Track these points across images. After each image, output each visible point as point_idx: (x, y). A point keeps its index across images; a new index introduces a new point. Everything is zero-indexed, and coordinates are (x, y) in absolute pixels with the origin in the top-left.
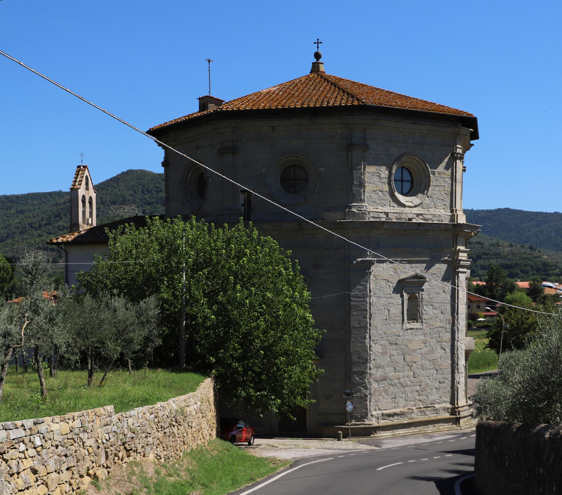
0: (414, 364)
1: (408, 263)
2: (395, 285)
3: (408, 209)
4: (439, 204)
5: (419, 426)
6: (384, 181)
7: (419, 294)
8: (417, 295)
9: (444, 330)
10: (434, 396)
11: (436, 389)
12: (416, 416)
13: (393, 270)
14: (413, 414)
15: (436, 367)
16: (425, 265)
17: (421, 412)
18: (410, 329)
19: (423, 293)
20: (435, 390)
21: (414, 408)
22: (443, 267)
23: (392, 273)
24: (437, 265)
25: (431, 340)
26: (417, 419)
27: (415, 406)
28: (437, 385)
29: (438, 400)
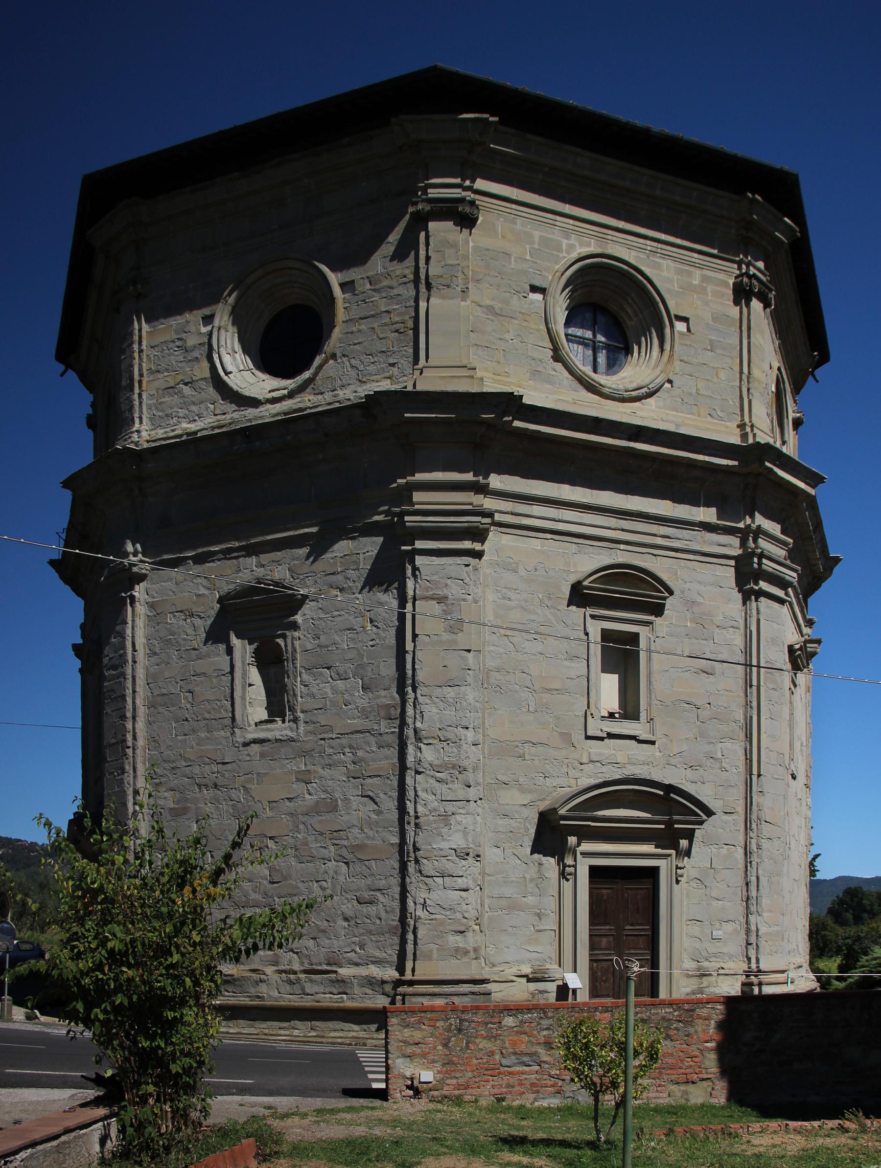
0: (271, 843)
1: (249, 555)
2: (209, 622)
3: (269, 406)
4: (372, 368)
5: (265, 1020)
6: (196, 354)
7: (284, 637)
8: (280, 641)
9: (372, 740)
10: (340, 940)
11: (346, 919)
12: (276, 994)
13: (205, 582)
14: (263, 988)
15: (344, 852)
16: (305, 550)
17: (290, 983)
18: (255, 741)
19: (296, 634)
20: (342, 923)
21: (269, 970)
22: (369, 548)
23: (203, 591)
24: (343, 547)
25: (327, 773)
26: (276, 1000)
27: (275, 963)
28: (349, 908)
29: (352, 955)
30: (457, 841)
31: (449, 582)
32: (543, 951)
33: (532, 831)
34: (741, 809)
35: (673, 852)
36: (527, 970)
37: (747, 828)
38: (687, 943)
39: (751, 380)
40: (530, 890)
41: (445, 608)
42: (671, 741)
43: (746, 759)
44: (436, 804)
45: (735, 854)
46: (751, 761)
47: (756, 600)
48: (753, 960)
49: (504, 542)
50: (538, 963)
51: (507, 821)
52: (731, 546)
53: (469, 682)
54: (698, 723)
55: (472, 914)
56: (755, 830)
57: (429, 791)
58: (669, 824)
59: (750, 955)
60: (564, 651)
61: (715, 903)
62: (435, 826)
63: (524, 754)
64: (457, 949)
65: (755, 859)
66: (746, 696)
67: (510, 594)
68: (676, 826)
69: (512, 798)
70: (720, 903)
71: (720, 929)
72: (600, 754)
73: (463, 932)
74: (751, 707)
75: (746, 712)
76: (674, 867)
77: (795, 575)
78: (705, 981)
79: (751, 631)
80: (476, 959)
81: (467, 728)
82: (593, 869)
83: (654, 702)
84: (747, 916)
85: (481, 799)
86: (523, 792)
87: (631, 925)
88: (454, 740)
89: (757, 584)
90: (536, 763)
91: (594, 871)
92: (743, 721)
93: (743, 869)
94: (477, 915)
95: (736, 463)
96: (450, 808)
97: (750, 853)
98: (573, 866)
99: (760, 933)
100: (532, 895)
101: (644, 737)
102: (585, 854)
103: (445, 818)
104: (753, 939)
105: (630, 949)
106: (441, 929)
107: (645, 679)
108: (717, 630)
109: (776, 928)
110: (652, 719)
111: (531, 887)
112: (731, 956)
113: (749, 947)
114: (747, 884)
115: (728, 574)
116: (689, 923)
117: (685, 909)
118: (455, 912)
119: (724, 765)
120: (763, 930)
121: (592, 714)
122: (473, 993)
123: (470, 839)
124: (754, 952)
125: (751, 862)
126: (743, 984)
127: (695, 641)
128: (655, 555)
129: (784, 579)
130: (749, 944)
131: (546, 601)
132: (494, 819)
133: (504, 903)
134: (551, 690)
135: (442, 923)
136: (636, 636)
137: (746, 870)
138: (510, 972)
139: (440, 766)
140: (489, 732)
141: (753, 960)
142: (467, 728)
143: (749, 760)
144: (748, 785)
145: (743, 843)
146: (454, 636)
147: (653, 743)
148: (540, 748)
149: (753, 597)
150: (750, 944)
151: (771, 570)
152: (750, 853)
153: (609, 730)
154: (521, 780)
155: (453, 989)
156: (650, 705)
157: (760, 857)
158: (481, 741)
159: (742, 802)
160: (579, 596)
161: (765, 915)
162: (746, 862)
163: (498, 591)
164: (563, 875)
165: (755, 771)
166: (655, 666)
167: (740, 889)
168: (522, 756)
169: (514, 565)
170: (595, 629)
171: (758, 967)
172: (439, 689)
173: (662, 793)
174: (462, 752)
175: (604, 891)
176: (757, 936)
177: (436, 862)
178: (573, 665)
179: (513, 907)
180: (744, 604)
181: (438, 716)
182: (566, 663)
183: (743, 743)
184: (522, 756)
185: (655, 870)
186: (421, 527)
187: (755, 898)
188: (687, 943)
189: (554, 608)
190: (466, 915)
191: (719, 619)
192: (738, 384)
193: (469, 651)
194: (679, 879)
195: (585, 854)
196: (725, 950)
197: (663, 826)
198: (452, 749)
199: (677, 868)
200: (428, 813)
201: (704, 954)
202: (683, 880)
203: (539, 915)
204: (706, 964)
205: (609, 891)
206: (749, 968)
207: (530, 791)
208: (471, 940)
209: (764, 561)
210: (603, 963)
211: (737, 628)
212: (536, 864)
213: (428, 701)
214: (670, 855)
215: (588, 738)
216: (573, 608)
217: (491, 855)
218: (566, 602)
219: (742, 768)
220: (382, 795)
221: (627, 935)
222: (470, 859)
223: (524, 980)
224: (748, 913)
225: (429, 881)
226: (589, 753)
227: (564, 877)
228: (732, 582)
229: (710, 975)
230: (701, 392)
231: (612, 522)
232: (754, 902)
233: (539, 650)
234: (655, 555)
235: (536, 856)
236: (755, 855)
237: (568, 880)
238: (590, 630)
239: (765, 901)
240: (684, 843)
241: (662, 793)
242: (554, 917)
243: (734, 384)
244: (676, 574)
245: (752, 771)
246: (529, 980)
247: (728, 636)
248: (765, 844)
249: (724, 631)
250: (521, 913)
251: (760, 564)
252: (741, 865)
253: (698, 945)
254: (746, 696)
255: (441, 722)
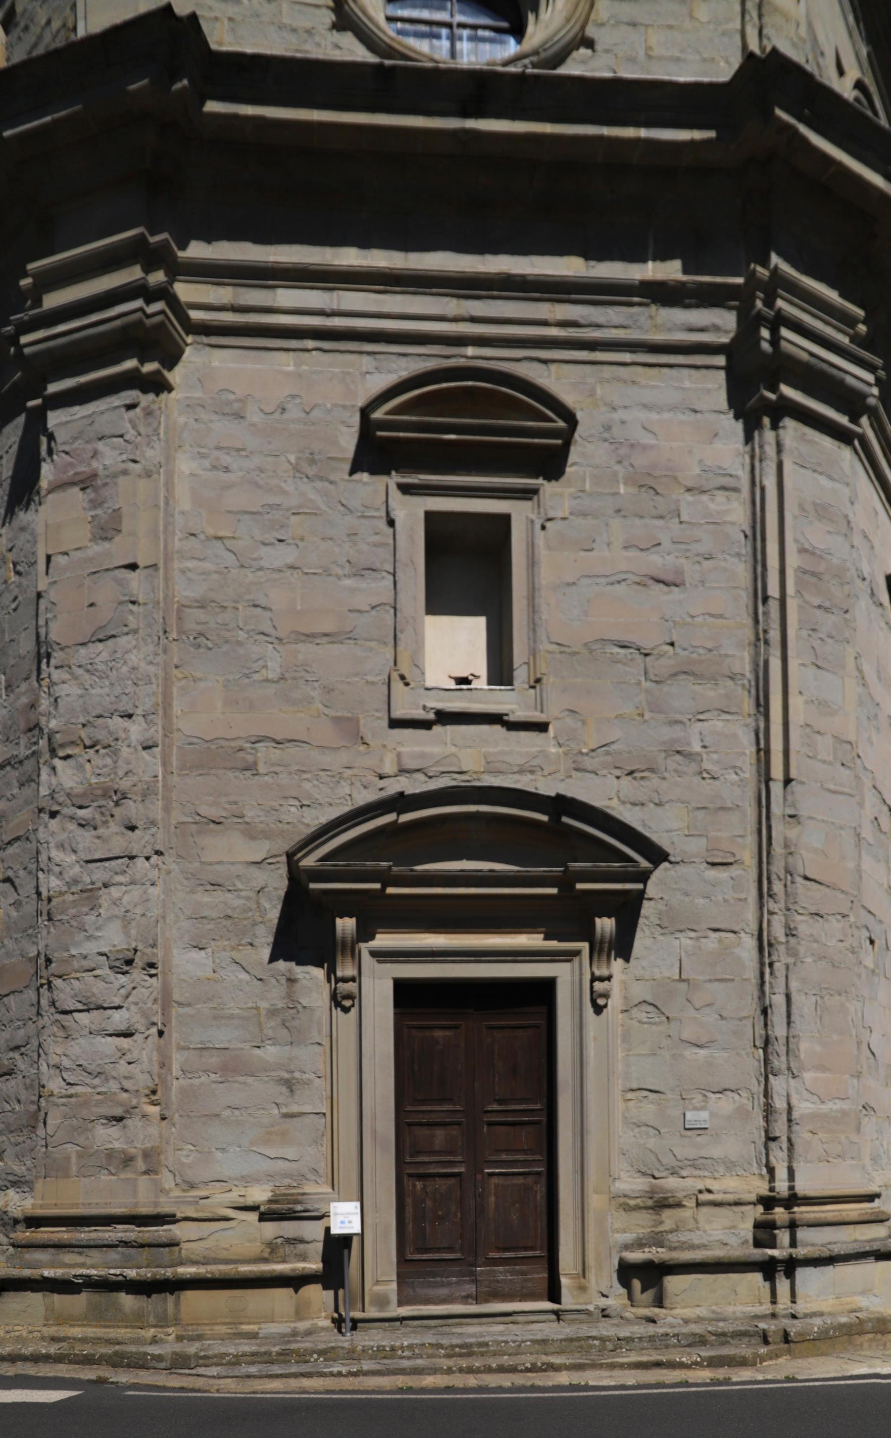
30: (113, 938)
31: (100, 446)
32: (299, 1156)
33: (274, 914)
34: (748, 856)
35: (585, 946)
36: (260, 1194)
37: (763, 893)
38: (624, 1137)
39: (765, 10)
40: (270, 1033)
41: (93, 496)
42: (584, 722)
43: (759, 750)
44: (77, 869)
45: (737, 951)
46: (767, 752)
47: (775, 427)
48: (781, 1173)
49: (215, 364)
50: (287, 1182)
51: (219, 896)
52: (716, 328)
53: (133, 626)
54: (646, 684)
55: (143, 1081)
56: (781, 895)
57: (66, 845)
58: (566, 882)
59: (773, 1161)
60: (343, 560)
61: (690, 1053)
62: (73, 911)
63: (255, 763)
64: (110, 1155)
65: (781, 958)
66: (756, 621)
67: (226, 459)
68: (580, 886)
69: (232, 851)
70: (702, 1052)
71: (703, 1108)
72: (422, 756)
73: (120, 1119)
74: (767, 642)
75: (757, 654)
76: (587, 977)
77: (870, 377)
78: (669, 1218)
79: (763, 489)
80: (146, 1173)
81: (130, 716)
82: (402, 987)
83: (544, 646)
84: (767, 1078)
85: (159, 853)
86: (253, 838)
87: (500, 1102)
88: (106, 742)
89: (774, 389)
90: (284, 779)
91: (405, 992)
92: (749, 675)
93: (754, 980)
94: (151, 1085)
95: (711, 134)
96: (99, 873)
97: (770, 945)
98: (353, 979)
99: (795, 1115)
100: (274, 1041)
101: (520, 715)
102: (381, 955)
103: (89, 895)
104: (780, 1128)
105: (499, 1151)
106: (84, 1113)
107: (524, 602)
108: (689, 497)
109: (838, 1105)
110: (538, 681)
111: (271, 1026)
112: (730, 1166)
113: (772, 1145)
114: (765, 1012)
115: (711, 387)
116: (630, 1095)
117: (620, 1067)
118: (107, 1080)
119: (707, 765)
120: (803, 1107)
121: (402, 677)
122: (126, 1244)
123: (133, 932)
124: (784, 1155)
125: (771, 965)
126: (758, 1225)
127: (637, 521)
128: (545, 362)
129: (842, 382)
130: (770, 1139)
131: (304, 466)
132: (192, 892)
133: (214, 1060)
134: (313, 636)
135: (85, 1104)
136: (505, 520)
137: (762, 983)
138: (220, 1200)
139: (84, 795)
140: (178, 723)
141: (781, 1173)
142: (130, 716)
143: (763, 753)
144: (763, 804)
145: (754, 927)
146: (107, 545)
147: (541, 727)
148: (292, 750)
149: (766, 421)
150: (774, 1139)
151: (805, 356)
152: (770, 945)
153: (440, 706)
154: (250, 814)
155: (93, 1235)
156: (534, 653)
157: (792, 952)
158: (159, 738)
159: (751, 840)
160: (375, 452)
161: (808, 1076)
162: (762, 964)
163: (203, 456)
164: (337, 1001)
165: (777, 772)
166: (546, 576)
167: (748, 1023)
168: (250, 768)
169: (236, 406)
170: (411, 513)
171: (791, 1188)
172: (83, 651)
173: (545, 818)
174: (120, 763)
175: (438, 1034)
176: (790, 1120)
177: (76, 983)
178: (363, 585)
179: (233, 1067)
180: (748, 438)
181: (81, 701)
182: (348, 582)
183: (751, 721)
184: (250, 768)
185: (548, 986)
186: (49, 351)
187: (782, 1041)
188: (624, 1137)
189: (321, 478)
190: (127, 1084)
191: (692, 472)
192: (738, 25)
193: (133, 567)
194: (601, 1002)
195: (381, 955)
196: (716, 1152)
197: (554, 891)
198: (102, 760)
199: (594, 979)
200: (65, 889)
201: (668, 1160)
202: (615, 1003)
203: (290, 1085)
204: (672, 1183)
205: (447, 1033)
206: (772, 1189)
207: (267, 835)
208: (141, 1134)
209: (785, 332)
210: (439, 1182)
211: (736, 490)
212: (283, 980)
213: (66, 676)
214: (577, 953)
215: (395, 724)
216: (365, 476)
217: (188, 964)
218: (347, 467)
219: (749, 772)
220: (22, 873)
221: (490, 1124)
222: (137, 974)
223: (253, 1217)
224: (768, 1071)
225: (66, 1019)
226: (399, 755)
227: (338, 1004)
228: (721, 398)
229: (679, 1205)
230: (656, 52)
231: (451, 306)
232: (782, 1049)
233: (290, 560)
234: (545, 362)
235: (281, 965)
236: (782, 949)
237: (346, 1010)
238: (399, 515)
239: (805, 1047)
240: (605, 925)
241: (545, 818)
242: (322, 1085)
243: (730, 26)
244: (592, 394)
245: (769, 774)
246: (264, 1217)
247: (712, 506)
248: (804, 926)
249: (704, 498)
250: (250, 1080)
251: (775, 340)
252: (751, 972)
253: (651, 1143)
254: (756, 621)
255: (85, 711)
